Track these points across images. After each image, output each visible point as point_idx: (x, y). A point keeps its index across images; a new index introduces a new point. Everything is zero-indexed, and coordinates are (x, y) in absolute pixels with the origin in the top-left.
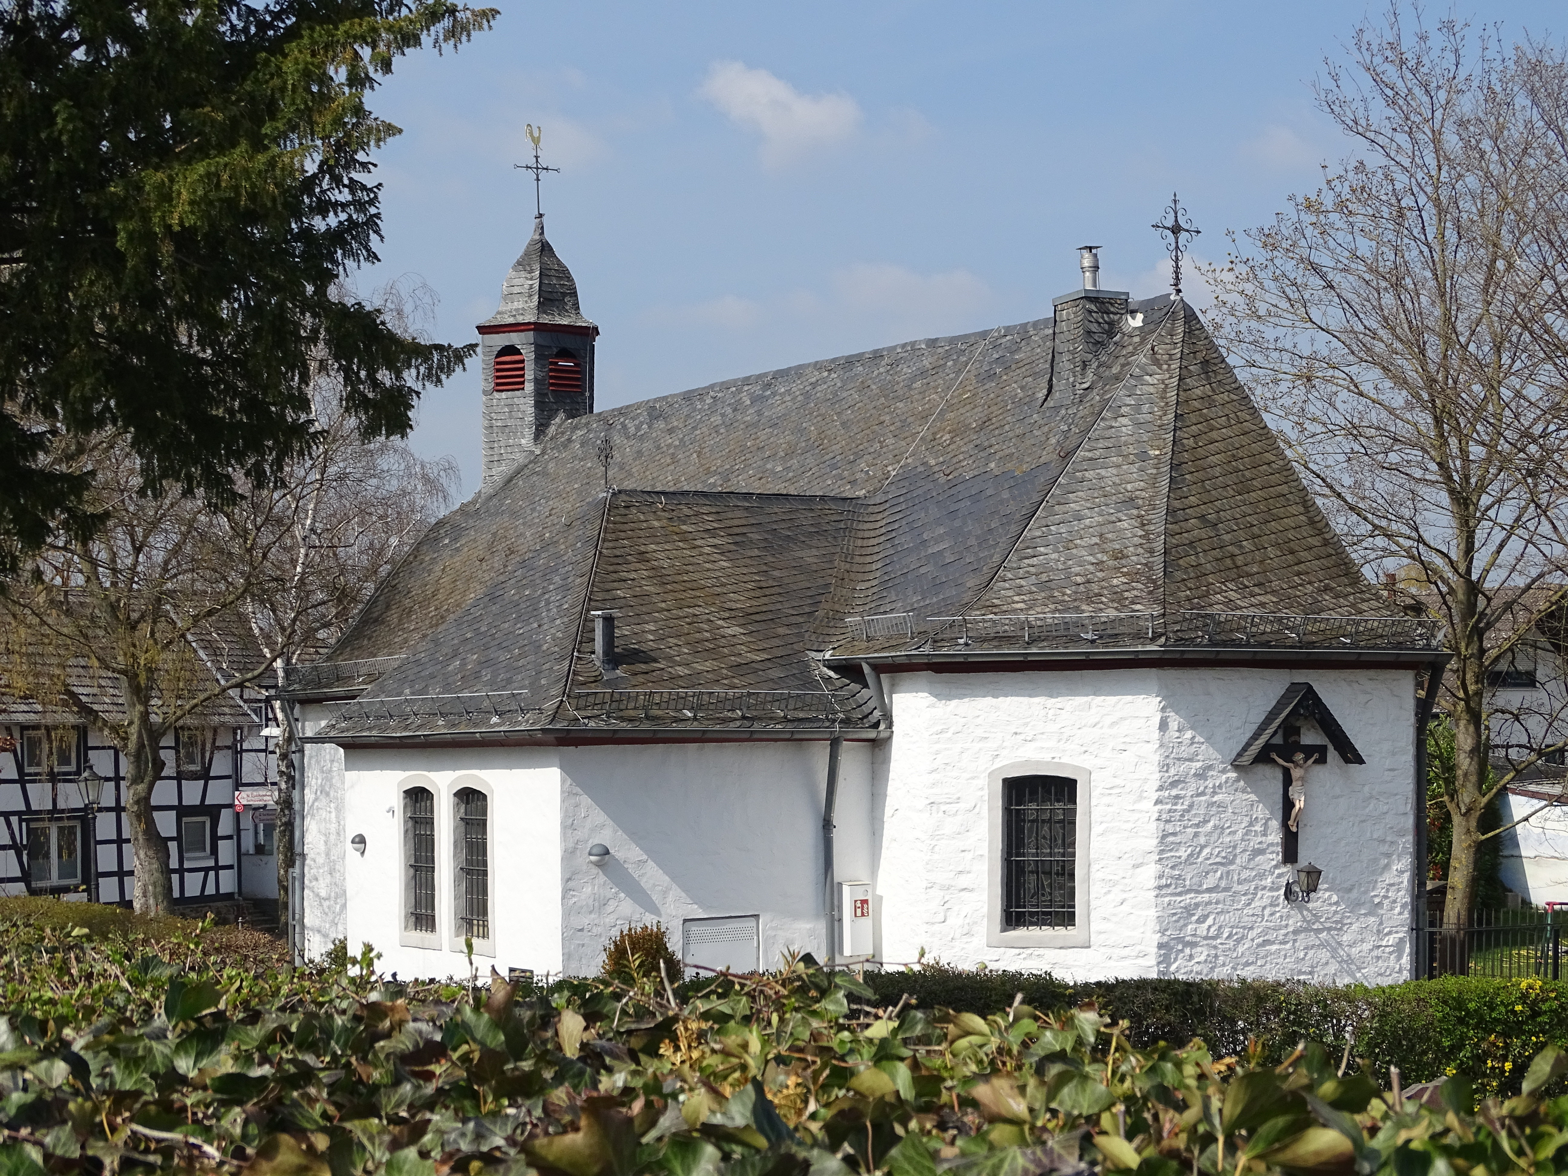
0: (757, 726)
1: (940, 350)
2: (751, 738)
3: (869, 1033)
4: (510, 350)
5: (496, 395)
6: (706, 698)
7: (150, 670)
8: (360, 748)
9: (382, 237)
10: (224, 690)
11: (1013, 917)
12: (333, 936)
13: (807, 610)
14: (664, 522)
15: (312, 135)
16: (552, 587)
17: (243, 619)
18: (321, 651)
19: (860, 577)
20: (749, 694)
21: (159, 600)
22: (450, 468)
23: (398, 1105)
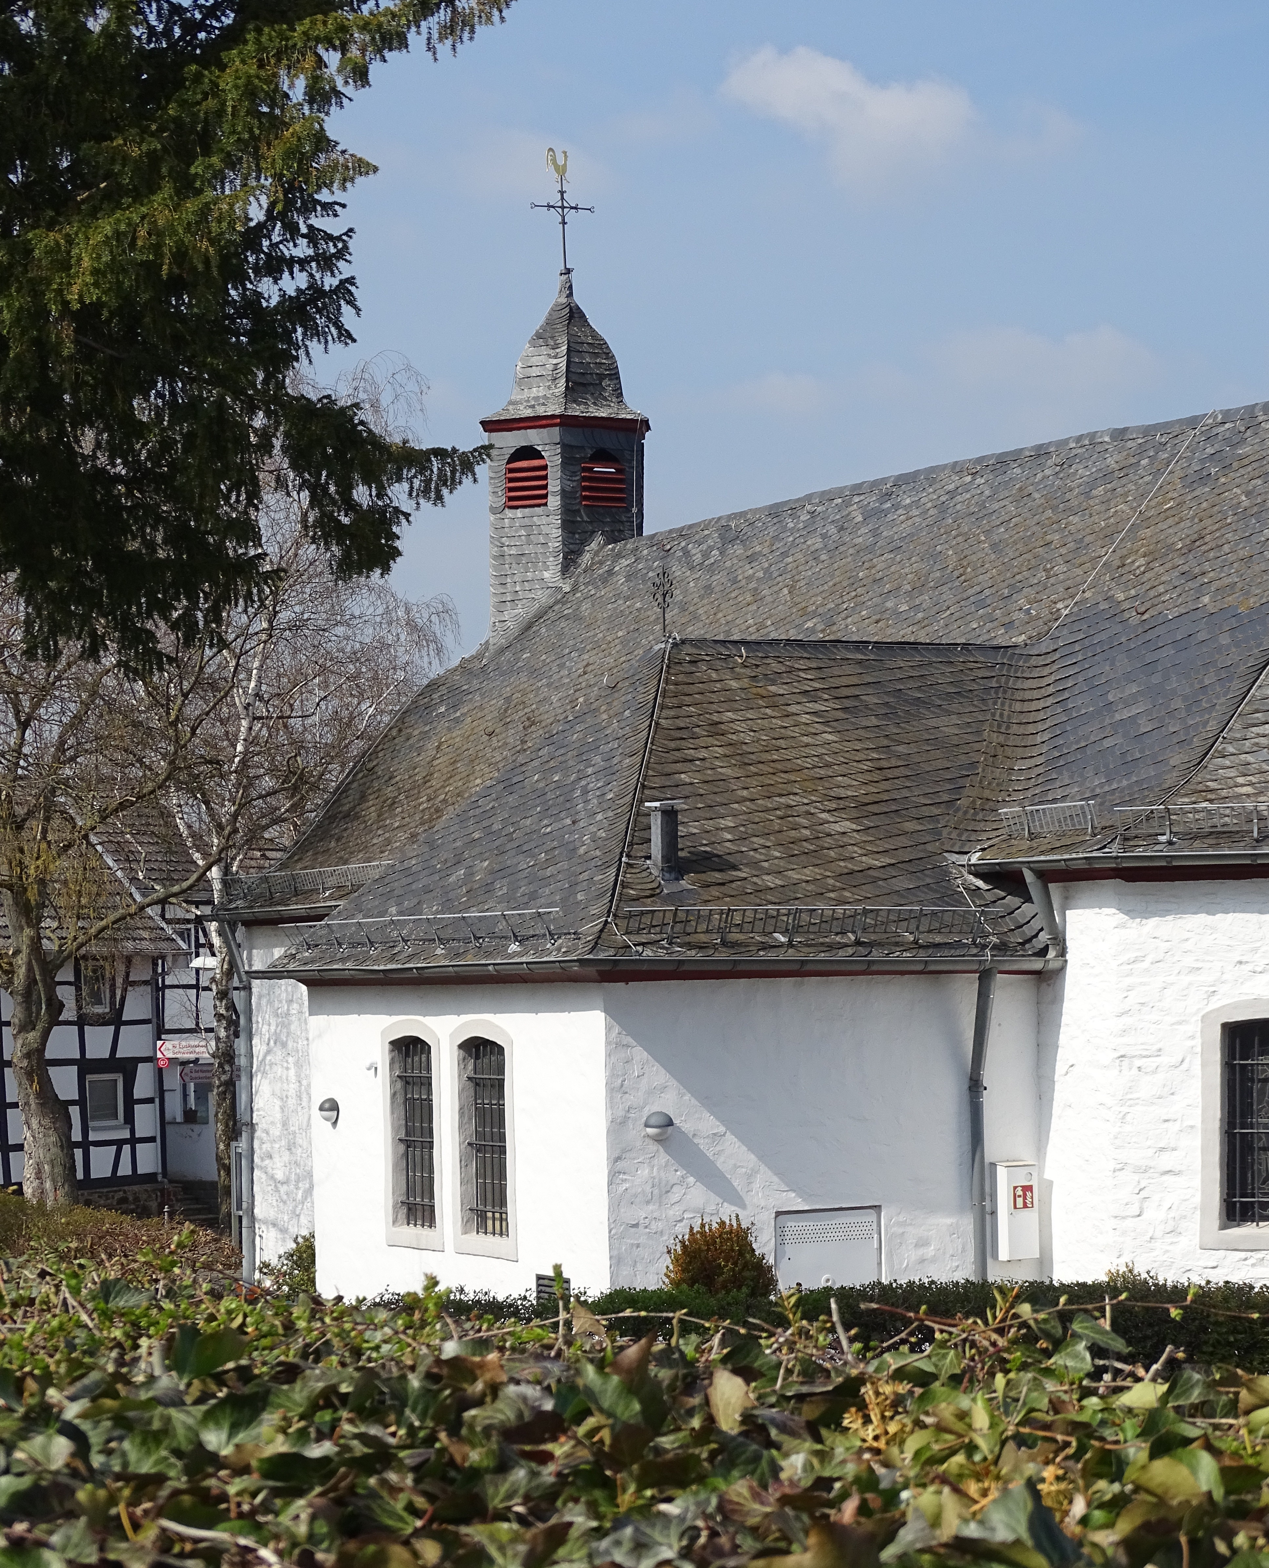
0: (876, 954)
1: (1130, 444)
2: (869, 970)
3: (1126, 1399)
4: (528, 452)
5: (509, 513)
6: (805, 917)
7: (42, 882)
8: (330, 986)
9: (358, 310)
10: (142, 908)
11: (1237, 1208)
12: (294, 1231)
13: (945, 797)
14: (745, 683)
15: (259, 171)
16: (590, 771)
17: (166, 815)
18: (269, 854)
19: (1020, 752)
20: (865, 912)
21: (53, 791)
22: (445, 611)
23: (510, 1496)
